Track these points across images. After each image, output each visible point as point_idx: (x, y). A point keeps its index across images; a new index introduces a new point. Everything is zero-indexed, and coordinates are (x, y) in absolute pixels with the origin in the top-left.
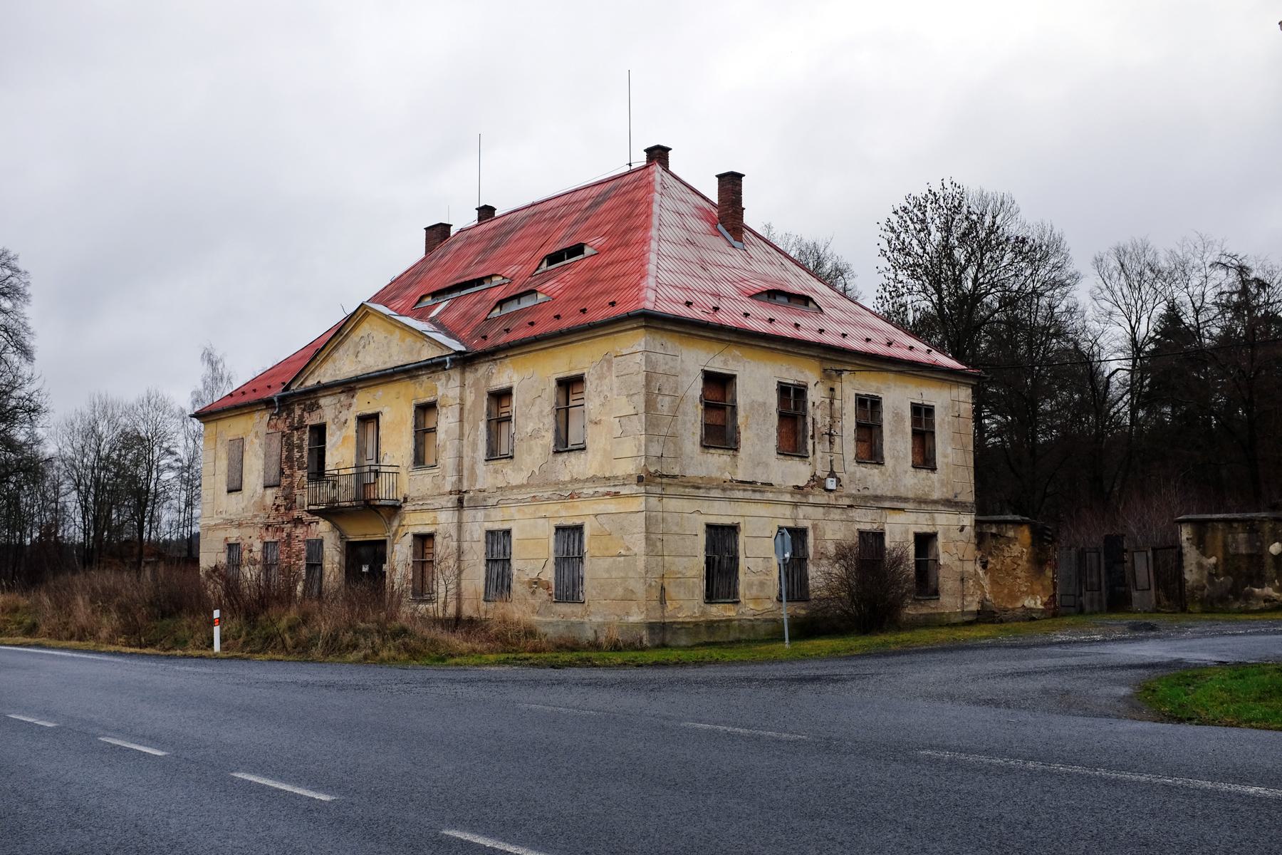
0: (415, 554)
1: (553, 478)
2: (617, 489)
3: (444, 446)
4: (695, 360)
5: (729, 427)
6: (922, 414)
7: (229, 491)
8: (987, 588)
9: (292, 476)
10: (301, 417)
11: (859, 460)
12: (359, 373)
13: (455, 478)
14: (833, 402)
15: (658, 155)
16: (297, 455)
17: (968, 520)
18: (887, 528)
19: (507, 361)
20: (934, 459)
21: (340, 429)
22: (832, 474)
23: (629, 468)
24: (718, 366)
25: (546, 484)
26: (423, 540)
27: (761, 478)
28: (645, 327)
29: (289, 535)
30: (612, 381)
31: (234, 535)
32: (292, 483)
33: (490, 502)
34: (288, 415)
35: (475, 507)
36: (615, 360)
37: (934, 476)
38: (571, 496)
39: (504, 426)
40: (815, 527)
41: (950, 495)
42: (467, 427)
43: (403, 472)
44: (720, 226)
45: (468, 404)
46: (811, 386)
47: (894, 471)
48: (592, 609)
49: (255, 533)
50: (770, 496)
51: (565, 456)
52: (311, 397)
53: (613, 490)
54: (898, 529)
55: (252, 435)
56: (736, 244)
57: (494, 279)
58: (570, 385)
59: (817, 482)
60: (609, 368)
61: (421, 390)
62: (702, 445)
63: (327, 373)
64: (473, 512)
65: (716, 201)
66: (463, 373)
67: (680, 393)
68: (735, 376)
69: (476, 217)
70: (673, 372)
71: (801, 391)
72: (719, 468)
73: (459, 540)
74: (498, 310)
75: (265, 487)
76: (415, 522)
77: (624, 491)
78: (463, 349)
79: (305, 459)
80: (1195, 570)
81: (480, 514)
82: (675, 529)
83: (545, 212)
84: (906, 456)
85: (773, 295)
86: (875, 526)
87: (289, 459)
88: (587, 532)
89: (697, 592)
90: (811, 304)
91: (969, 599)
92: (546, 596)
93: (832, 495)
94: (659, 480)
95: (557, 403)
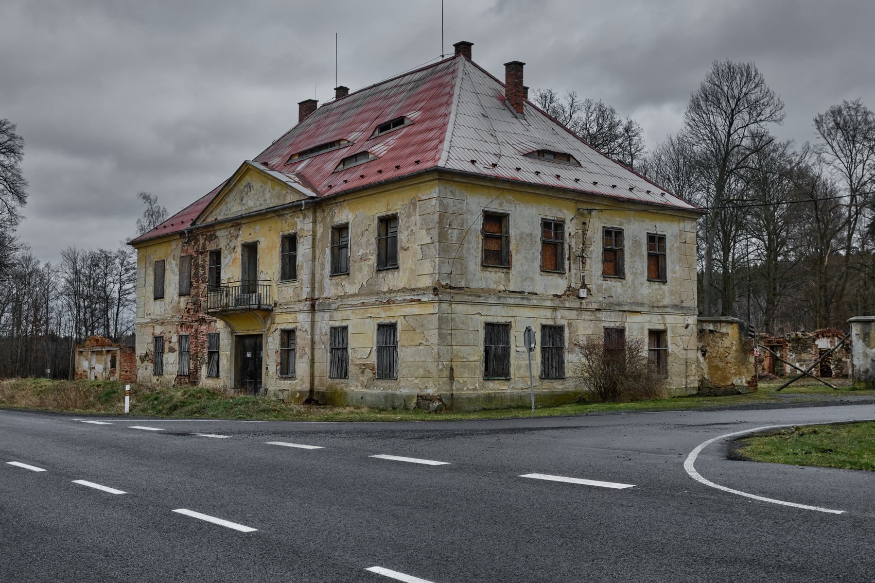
0: (282, 344)
1: (376, 289)
2: (419, 297)
3: (302, 266)
4: (475, 205)
5: (504, 251)
6: (656, 242)
7: (155, 299)
8: (706, 370)
9: (197, 287)
10: (204, 244)
11: (606, 275)
12: (244, 212)
13: (309, 289)
14: (587, 235)
15: (464, 49)
16: (201, 272)
17: (692, 320)
18: (626, 325)
19: (345, 204)
20: (665, 274)
21: (230, 254)
22: (584, 286)
23: (426, 282)
24: (495, 207)
25: (371, 294)
26: (288, 335)
27: (528, 289)
28: (439, 179)
29: (196, 331)
30: (416, 218)
31: (158, 330)
32: (198, 293)
33: (333, 306)
34: (195, 243)
35: (323, 310)
36: (418, 203)
37: (665, 288)
38: (389, 302)
39: (344, 251)
40: (570, 325)
41: (677, 302)
42: (318, 252)
43: (274, 284)
44: (507, 102)
45: (319, 235)
46: (568, 221)
47: (633, 283)
48: (402, 384)
49: (173, 329)
50: (535, 302)
51: (384, 273)
52: (210, 231)
53: (416, 298)
54: (635, 326)
55: (171, 257)
56: (518, 115)
57: (342, 143)
58: (388, 222)
59: (571, 292)
60: (415, 210)
61: (285, 227)
62: (482, 265)
63: (221, 213)
64: (322, 314)
65: (504, 81)
66: (315, 213)
67: (465, 227)
68: (508, 215)
69: (335, 95)
70: (460, 211)
71: (559, 225)
72: (496, 282)
73: (312, 334)
74: (341, 166)
75: (180, 295)
76: (283, 321)
77: (424, 299)
78: (314, 195)
79: (207, 276)
80: (861, 358)
81: (327, 315)
82: (461, 326)
83: (381, 91)
84: (642, 272)
85: (542, 154)
86: (618, 324)
87: (196, 274)
88: (399, 328)
89: (478, 372)
90: (572, 160)
91: (692, 378)
92: (371, 375)
93: (584, 301)
94: (449, 290)
95: (379, 235)
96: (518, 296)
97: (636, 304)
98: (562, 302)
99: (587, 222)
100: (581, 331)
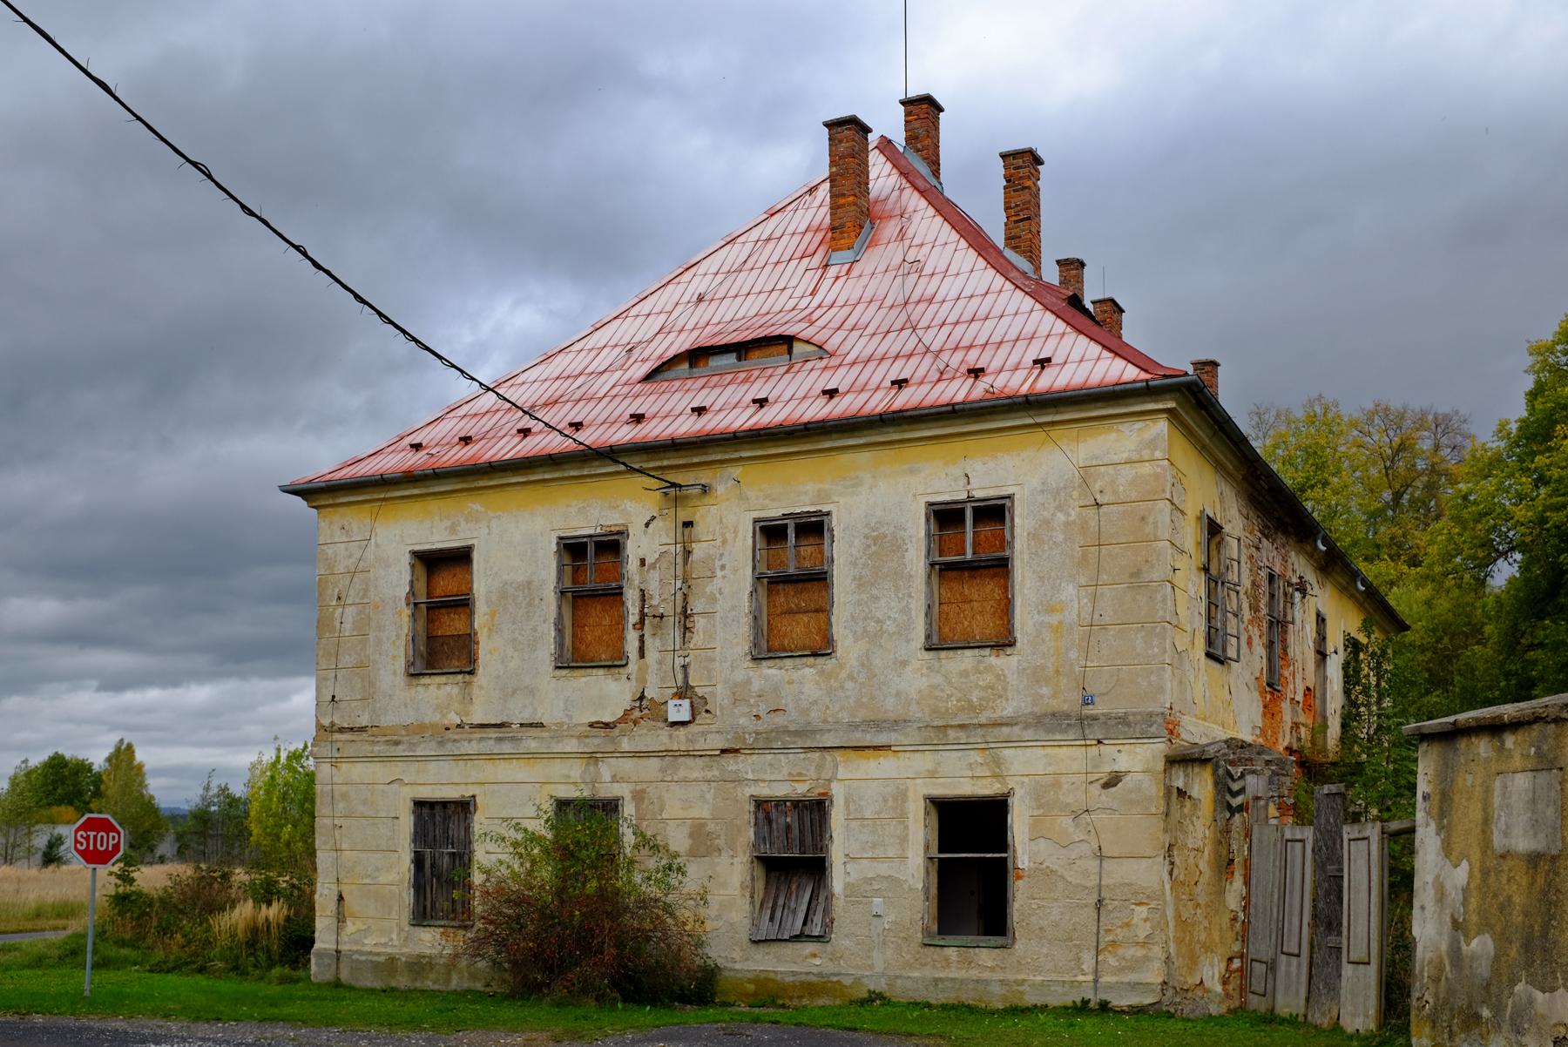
18: (838, 792)
22: (684, 691)
24: (439, 538)
50: (533, 745)
58: (443, 565)
59: (644, 708)
82: (361, 808)
96: (493, 733)
97: (876, 724)
98: (613, 740)
99: (697, 519)
100: (673, 810)
